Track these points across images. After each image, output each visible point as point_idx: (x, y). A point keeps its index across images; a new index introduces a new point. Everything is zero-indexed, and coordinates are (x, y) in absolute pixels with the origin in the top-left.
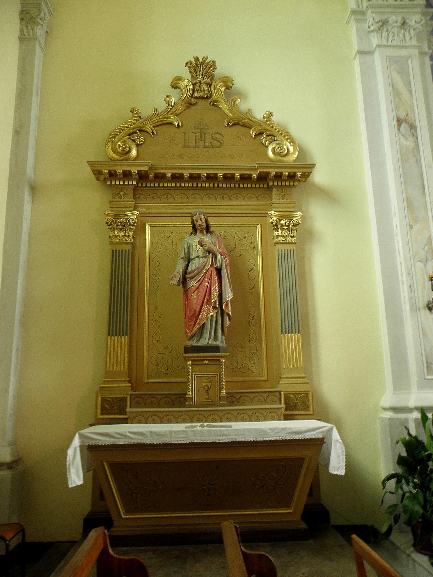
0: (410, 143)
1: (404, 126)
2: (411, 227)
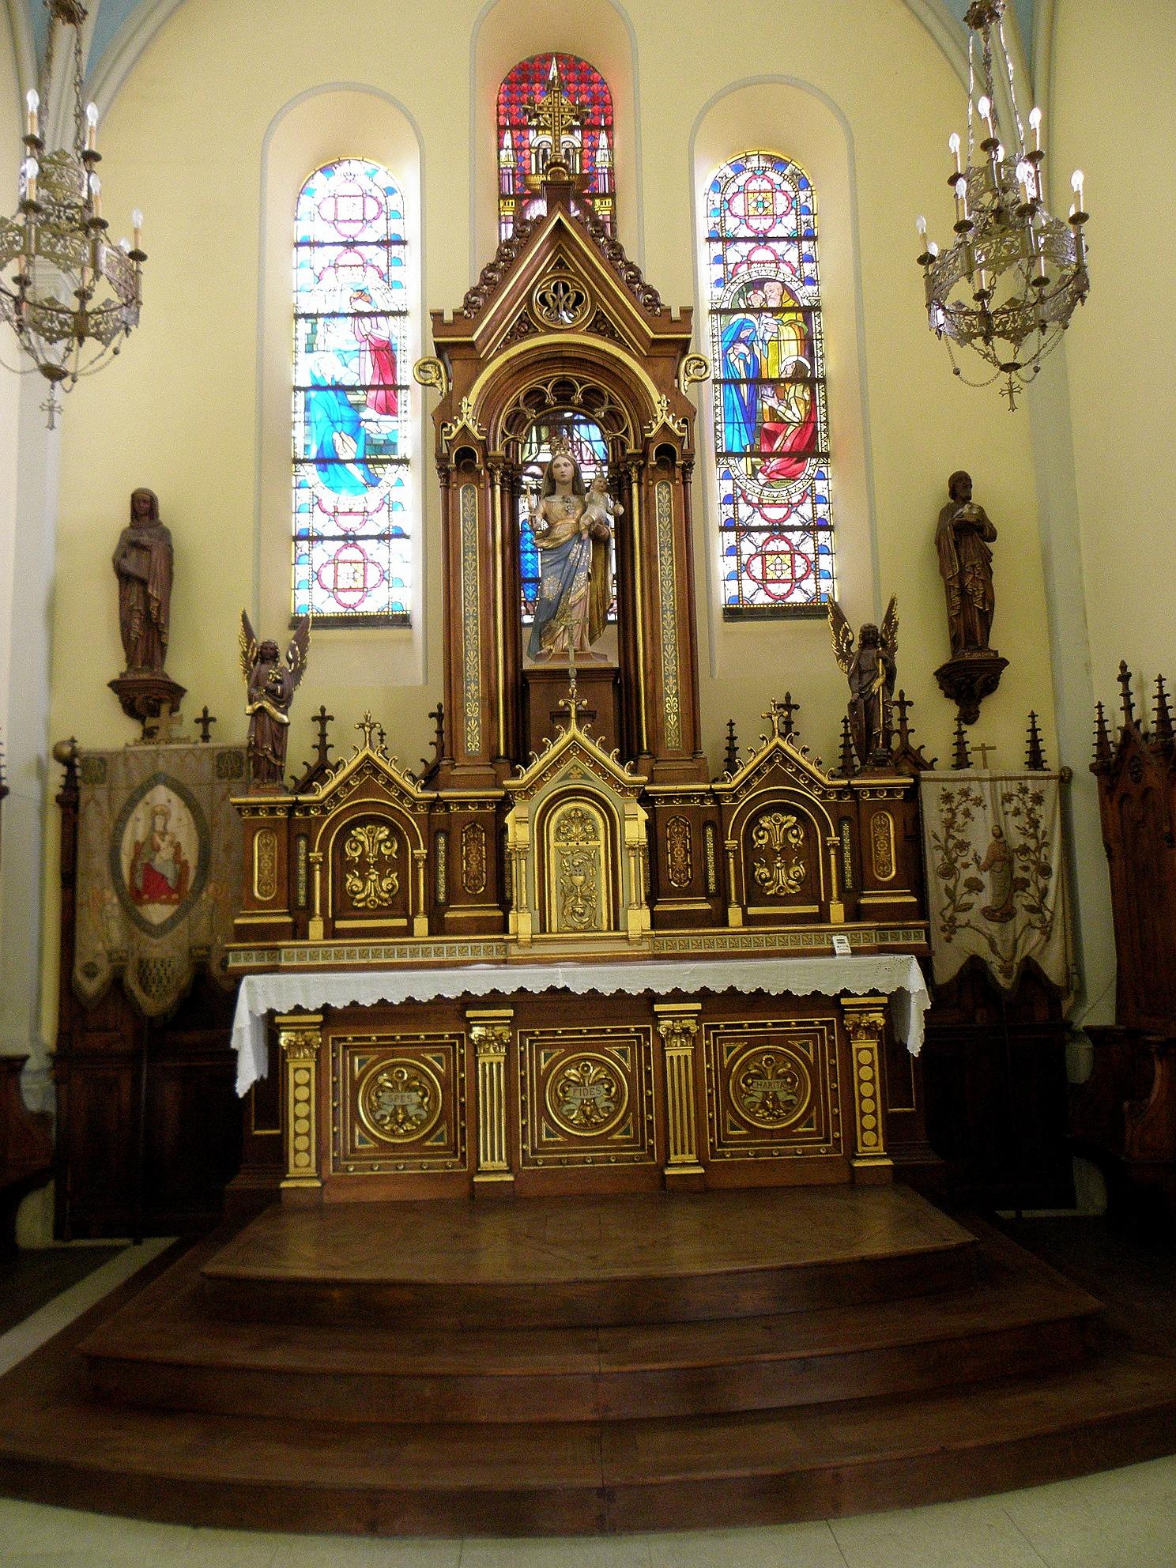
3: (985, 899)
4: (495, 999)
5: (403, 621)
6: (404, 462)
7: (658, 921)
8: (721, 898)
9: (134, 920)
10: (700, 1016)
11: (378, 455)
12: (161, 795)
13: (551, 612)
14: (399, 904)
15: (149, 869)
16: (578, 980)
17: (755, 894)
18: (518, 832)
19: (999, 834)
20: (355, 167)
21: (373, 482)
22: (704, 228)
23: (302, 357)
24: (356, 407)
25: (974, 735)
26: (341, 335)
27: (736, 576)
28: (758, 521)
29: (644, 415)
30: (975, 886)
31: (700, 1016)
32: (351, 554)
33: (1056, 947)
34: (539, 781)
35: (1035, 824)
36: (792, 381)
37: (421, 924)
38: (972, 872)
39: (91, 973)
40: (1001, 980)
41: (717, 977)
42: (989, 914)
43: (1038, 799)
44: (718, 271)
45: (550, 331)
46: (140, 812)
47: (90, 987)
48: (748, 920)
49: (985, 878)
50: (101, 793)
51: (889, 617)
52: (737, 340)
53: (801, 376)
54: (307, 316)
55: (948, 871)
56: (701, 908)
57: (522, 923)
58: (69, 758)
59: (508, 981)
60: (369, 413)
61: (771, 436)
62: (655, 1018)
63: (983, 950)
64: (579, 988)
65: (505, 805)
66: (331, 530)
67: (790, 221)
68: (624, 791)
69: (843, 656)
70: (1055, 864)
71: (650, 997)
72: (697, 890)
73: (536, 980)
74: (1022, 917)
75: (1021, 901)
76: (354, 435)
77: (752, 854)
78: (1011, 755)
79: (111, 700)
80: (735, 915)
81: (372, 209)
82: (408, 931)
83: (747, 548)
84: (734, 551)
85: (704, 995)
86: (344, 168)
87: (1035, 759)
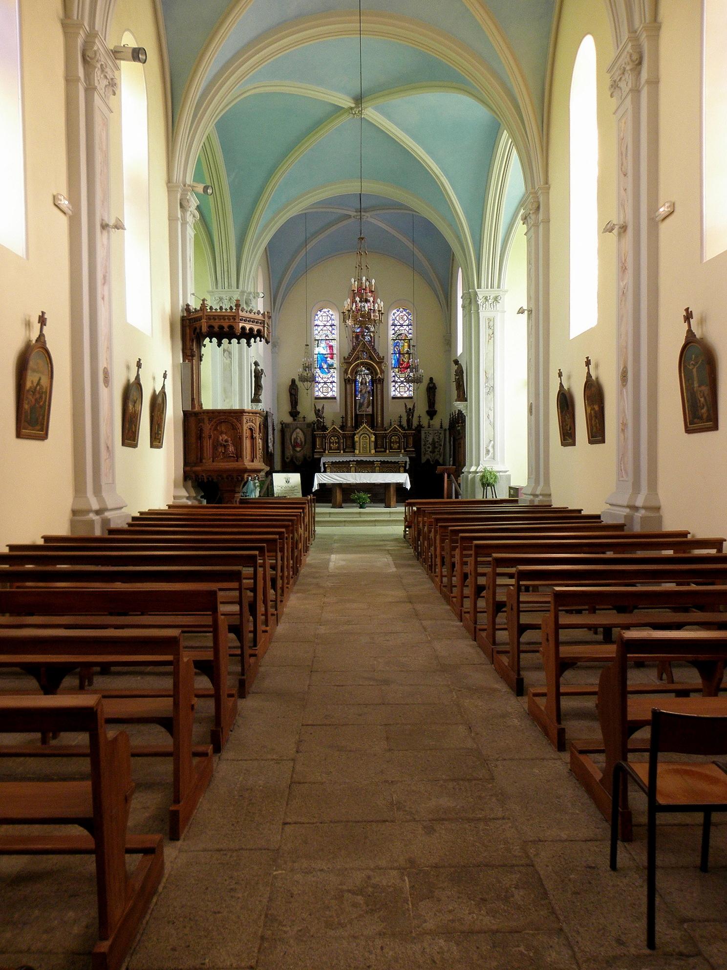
0: (228, 361)
1: (226, 353)
2: (224, 401)
3: (430, 450)
4: (354, 461)
5: (335, 398)
6: (335, 368)
7: (376, 452)
8: (386, 449)
9: (294, 450)
10: (380, 464)
11: (330, 366)
12: (298, 430)
13: (361, 405)
14: (338, 449)
15: (297, 442)
16: (364, 459)
17: (391, 448)
18: (356, 439)
19: (433, 439)
20: (325, 310)
21: (329, 372)
22: (391, 322)
23: (316, 348)
24: (327, 358)
25: (432, 422)
26: (323, 344)
27: (394, 391)
28: (399, 381)
29: (377, 374)
30: (429, 448)
31: (380, 464)
32: (325, 386)
33: (442, 458)
34: (359, 432)
35: (440, 437)
36: (406, 354)
37: (342, 452)
38: (429, 445)
39: (287, 458)
40: (432, 463)
41: (382, 459)
42: (431, 452)
43: (440, 433)
44: (393, 332)
45: (361, 359)
46: (295, 433)
47: (288, 460)
48: (390, 452)
49: (430, 446)
50: (289, 430)
51: (414, 406)
52: (396, 345)
53: (408, 353)
54: (317, 340)
55: (424, 445)
56: (708, 565)
57: (357, 452)
58: (282, 424)
59: (355, 459)
60: (329, 359)
61: (402, 364)
62: (374, 464)
63: (429, 458)
64: (364, 460)
65: (355, 434)
66: (322, 381)
67: (407, 322)
68: (371, 433)
69: (406, 412)
70: (442, 444)
71: (374, 461)
72: (382, 447)
73: (359, 459)
74: (436, 453)
75: (436, 450)
76: (326, 363)
77: (391, 442)
78: (438, 426)
79: (288, 414)
80: (388, 451)
81: (329, 319)
82: (340, 452)
83: (397, 386)
84: (394, 386)
85: (381, 461)
86: (324, 310)
87: (441, 427)
